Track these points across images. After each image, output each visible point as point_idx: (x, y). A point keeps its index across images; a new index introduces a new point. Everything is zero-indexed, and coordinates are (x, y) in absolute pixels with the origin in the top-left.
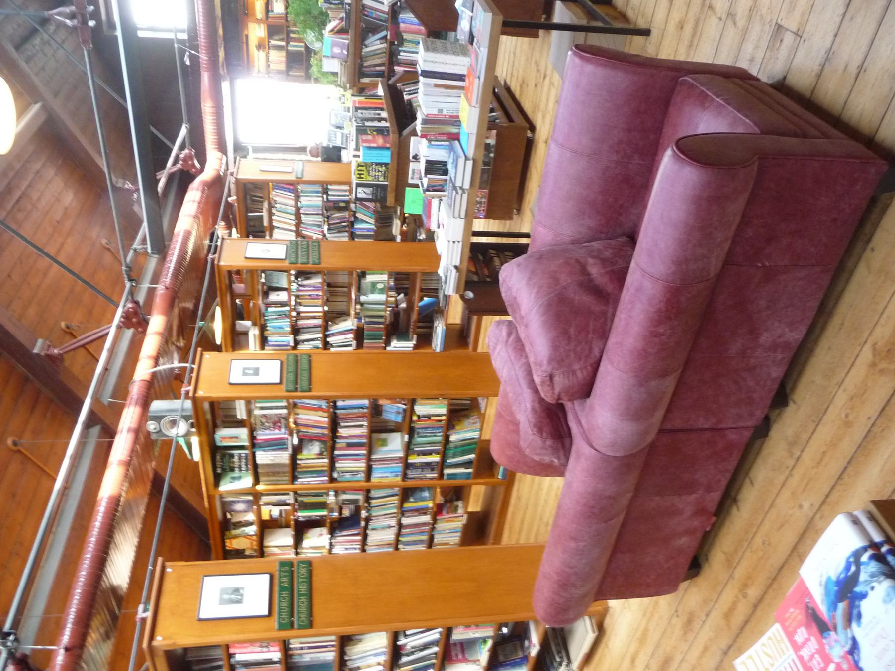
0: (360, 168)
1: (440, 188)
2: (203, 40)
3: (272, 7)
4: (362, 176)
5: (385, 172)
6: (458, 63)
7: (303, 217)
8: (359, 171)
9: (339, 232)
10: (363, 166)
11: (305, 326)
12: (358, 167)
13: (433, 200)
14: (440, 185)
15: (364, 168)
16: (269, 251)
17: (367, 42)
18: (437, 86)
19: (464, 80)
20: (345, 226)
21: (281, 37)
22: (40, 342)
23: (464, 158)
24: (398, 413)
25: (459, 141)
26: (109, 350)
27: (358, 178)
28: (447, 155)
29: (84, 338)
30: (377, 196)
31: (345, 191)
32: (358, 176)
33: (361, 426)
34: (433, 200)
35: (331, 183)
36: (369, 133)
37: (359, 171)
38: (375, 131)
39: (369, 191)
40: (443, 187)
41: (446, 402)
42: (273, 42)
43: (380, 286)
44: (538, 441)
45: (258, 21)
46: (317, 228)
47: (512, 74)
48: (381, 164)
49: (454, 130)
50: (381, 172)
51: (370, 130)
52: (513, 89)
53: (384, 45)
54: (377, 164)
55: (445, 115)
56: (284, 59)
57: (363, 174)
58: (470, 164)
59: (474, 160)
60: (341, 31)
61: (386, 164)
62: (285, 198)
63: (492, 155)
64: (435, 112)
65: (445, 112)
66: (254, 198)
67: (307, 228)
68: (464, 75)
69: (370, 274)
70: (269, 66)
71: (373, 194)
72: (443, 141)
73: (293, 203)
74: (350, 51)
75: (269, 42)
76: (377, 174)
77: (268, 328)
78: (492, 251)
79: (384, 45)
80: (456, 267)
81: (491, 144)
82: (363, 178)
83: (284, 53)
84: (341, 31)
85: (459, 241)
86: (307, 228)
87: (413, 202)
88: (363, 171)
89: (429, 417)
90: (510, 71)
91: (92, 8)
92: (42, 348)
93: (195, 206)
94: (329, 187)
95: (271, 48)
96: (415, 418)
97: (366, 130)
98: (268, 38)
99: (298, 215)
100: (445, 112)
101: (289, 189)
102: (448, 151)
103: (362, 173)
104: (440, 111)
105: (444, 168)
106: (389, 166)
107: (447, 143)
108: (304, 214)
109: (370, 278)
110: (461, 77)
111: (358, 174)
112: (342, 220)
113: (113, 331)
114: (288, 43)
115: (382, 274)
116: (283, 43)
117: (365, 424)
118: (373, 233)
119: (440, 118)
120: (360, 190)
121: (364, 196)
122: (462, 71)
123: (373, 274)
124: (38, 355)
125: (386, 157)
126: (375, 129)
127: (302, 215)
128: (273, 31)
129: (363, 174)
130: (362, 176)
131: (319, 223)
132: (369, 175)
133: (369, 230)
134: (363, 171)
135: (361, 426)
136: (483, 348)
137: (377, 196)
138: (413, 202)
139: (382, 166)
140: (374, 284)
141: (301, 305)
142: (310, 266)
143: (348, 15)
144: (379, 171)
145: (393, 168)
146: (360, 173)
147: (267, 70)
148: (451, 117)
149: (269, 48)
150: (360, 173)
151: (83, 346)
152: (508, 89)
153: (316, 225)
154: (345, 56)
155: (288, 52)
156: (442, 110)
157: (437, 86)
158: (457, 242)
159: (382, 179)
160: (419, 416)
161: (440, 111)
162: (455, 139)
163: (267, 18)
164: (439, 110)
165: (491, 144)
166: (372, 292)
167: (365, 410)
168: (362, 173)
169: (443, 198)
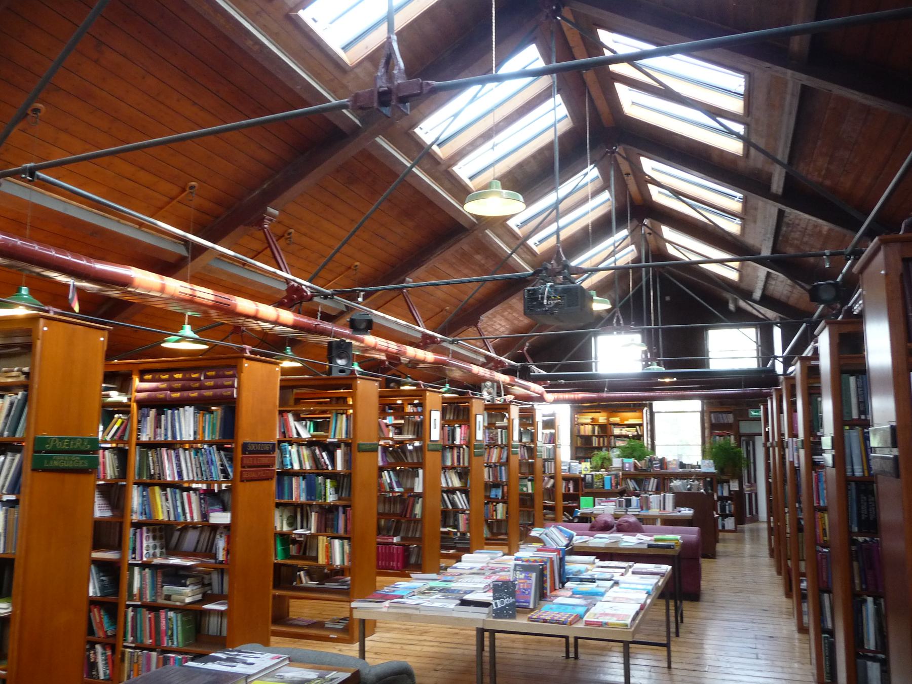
3: (617, 428)
17: (632, 481)
18: (660, 500)
21: (600, 432)
22: (276, 212)
24: (496, 496)
26: (275, 273)
29: (278, 246)
31: (551, 471)
33: (489, 478)
35: (555, 463)
41: (504, 518)
42: (596, 428)
44: (604, 519)
45: (608, 419)
53: (632, 489)
56: (587, 434)
60: (635, 466)
61: (603, 488)
64: (651, 500)
69: (532, 484)
75: (596, 425)
79: (632, 489)
83: (590, 434)
84: (635, 466)
87: (586, 501)
89: (496, 511)
91: (770, 480)
92: (270, 215)
93: (483, 374)
94: (553, 463)
96: (494, 504)
104: (651, 502)
110: (664, 509)
113: (421, 329)
114: (596, 436)
116: (596, 433)
117: (491, 480)
120: (590, 476)
124: (265, 211)
125: (607, 487)
128: (603, 427)
135: (489, 478)
136: (381, 581)
138: (586, 501)
142: (473, 450)
143: (645, 470)
145: (602, 490)
151: (270, 246)
155: (592, 436)
157: (660, 500)
160: (495, 505)
163: (611, 424)
167: (499, 480)
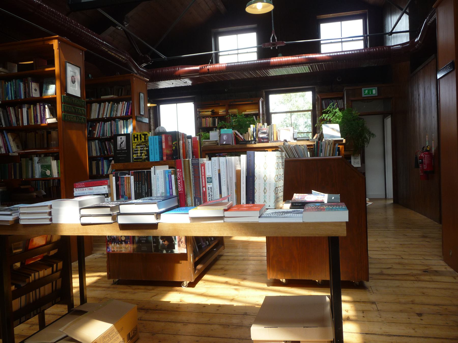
0: (143, 136)
1: (121, 193)
2: (216, 66)
4: (136, 139)
5: (141, 159)
6: (267, 194)
7: (108, 124)
8: (140, 135)
9: (100, 149)
10: (145, 139)
11: (9, 113)
12: (143, 135)
13: (106, 186)
14: (124, 192)
15: (143, 140)
16: (73, 82)
19: (247, 202)
20: (104, 153)
23: (158, 211)
25: (177, 207)
27: (134, 135)
28: (159, 195)
30: (119, 154)
32: (136, 136)
34: (106, 186)
36: (174, 143)
37: (140, 135)
38: (176, 147)
39: (124, 146)
40: (123, 197)
43: (48, 172)
46: (101, 133)
47: (229, 260)
48: (148, 155)
49: (189, 200)
50: (141, 156)
51: (176, 143)
52: (219, 262)
54: (148, 151)
55: (205, 187)
57: (138, 140)
58: (151, 220)
59: (154, 226)
62: (122, 110)
63: (165, 252)
65: (209, 185)
66: (120, 90)
67: (101, 126)
68: (253, 202)
69: (57, 163)
70: (204, 118)
71: (122, 150)
72: (177, 188)
73: (119, 115)
74: (226, 146)
75: (216, 117)
76: (139, 152)
77: (7, 83)
78: (60, 265)
80: (17, 220)
81: (174, 250)
82: (134, 140)
85: (51, 220)
86: (101, 126)
88: (141, 140)
90: (230, 258)
95: (213, 118)
97: (176, 140)
98: (218, 117)
99: (110, 119)
100: (209, 185)
101: (128, 112)
102: (164, 195)
103: (139, 139)
104: (210, 180)
105: (144, 195)
106: (147, 161)
107: (174, 194)
108: (111, 123)
109: (54, 164)
111: (137, 135)
112: (108, 151)
115: (58, 173)
118: (101, 173)
119: (202, 181)
121: (119, 143)
122: (259, 198)
123: (58, 166)
126: (178, 148)
127: (110, 122)
129: (138, 140)
130: (136, 139)
131: (105, 134)
132: (137, 145)
133: (103, 170)
134: (141, 140)
137: (119, 154)
139: (146, 155)
140: (49, 167)
141: (28, 109)
144: (141, 153)
146: (139, 137)
147: (201, 117)
148: (205, 193)
149: (213, 117)
150: (139, 137)
152: (216, 260)
153: (104, 133)
154: (222, 143)
156: (211, 182)
158: (50, 217)
159: (135, 156)
161: (210, 180)
162: (179, 201)
164: (211, 178)
165: (174, 250)
166: (42, 167)
168: (139, 139)
169: (109, 199)
